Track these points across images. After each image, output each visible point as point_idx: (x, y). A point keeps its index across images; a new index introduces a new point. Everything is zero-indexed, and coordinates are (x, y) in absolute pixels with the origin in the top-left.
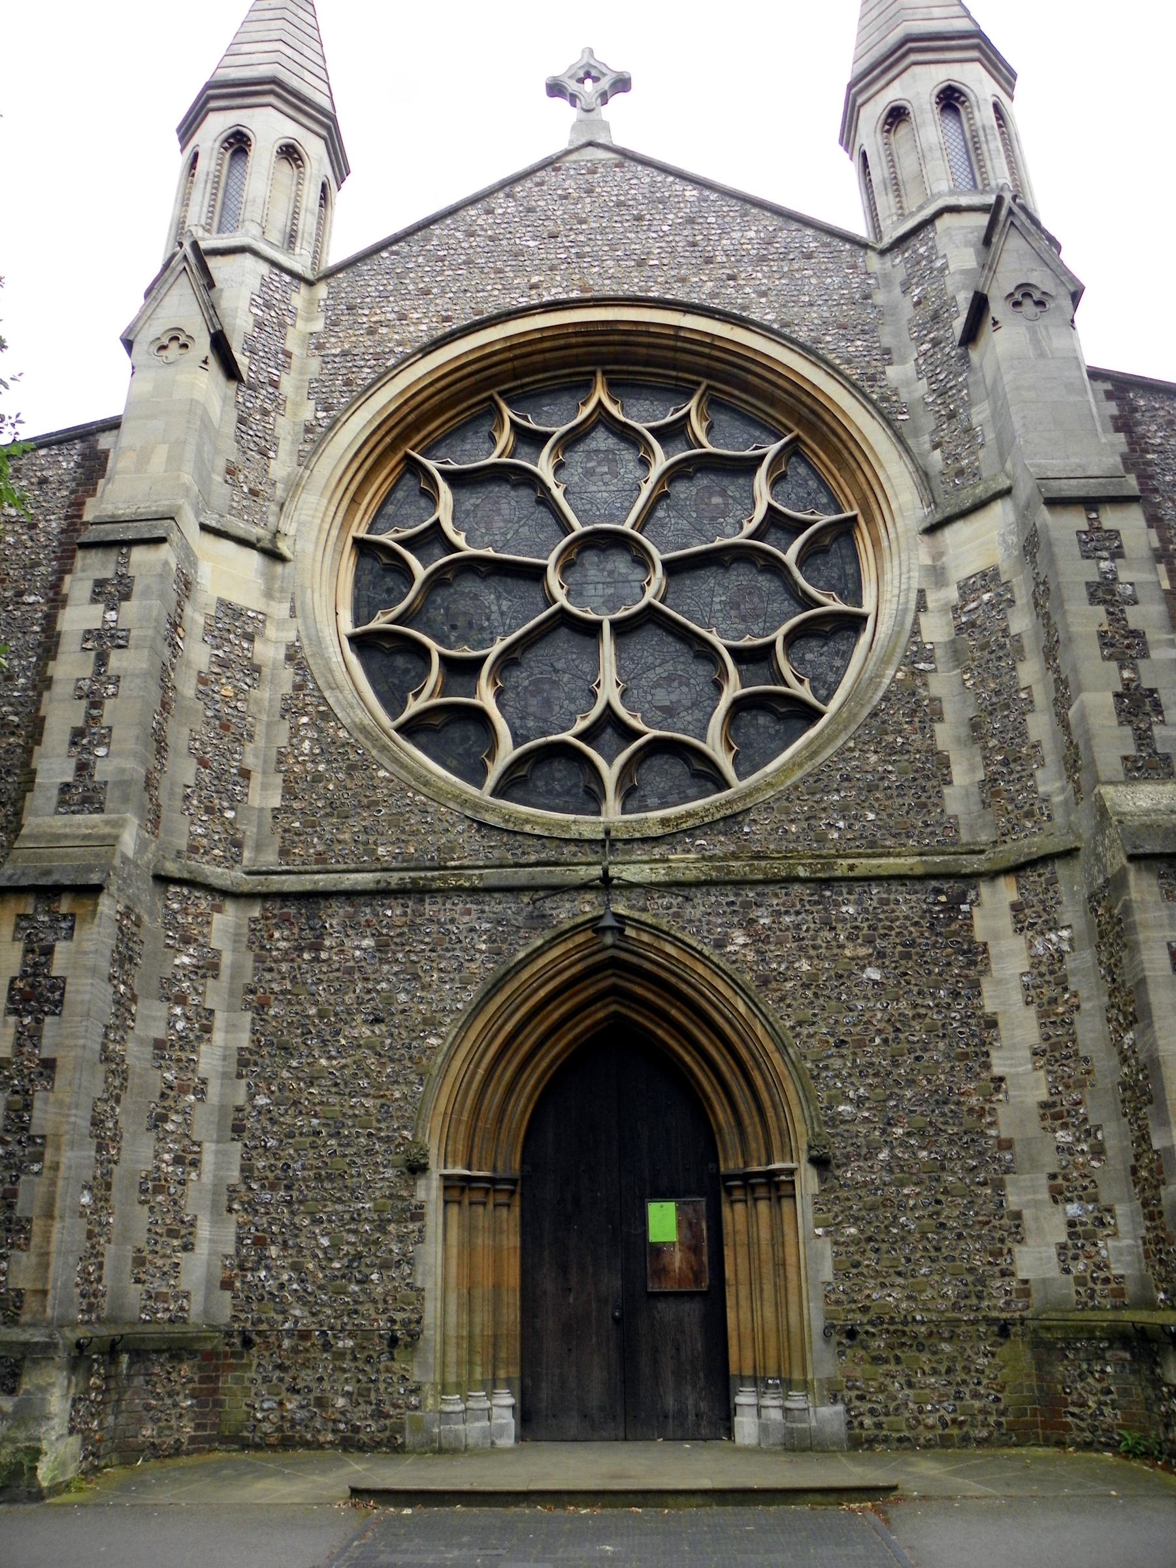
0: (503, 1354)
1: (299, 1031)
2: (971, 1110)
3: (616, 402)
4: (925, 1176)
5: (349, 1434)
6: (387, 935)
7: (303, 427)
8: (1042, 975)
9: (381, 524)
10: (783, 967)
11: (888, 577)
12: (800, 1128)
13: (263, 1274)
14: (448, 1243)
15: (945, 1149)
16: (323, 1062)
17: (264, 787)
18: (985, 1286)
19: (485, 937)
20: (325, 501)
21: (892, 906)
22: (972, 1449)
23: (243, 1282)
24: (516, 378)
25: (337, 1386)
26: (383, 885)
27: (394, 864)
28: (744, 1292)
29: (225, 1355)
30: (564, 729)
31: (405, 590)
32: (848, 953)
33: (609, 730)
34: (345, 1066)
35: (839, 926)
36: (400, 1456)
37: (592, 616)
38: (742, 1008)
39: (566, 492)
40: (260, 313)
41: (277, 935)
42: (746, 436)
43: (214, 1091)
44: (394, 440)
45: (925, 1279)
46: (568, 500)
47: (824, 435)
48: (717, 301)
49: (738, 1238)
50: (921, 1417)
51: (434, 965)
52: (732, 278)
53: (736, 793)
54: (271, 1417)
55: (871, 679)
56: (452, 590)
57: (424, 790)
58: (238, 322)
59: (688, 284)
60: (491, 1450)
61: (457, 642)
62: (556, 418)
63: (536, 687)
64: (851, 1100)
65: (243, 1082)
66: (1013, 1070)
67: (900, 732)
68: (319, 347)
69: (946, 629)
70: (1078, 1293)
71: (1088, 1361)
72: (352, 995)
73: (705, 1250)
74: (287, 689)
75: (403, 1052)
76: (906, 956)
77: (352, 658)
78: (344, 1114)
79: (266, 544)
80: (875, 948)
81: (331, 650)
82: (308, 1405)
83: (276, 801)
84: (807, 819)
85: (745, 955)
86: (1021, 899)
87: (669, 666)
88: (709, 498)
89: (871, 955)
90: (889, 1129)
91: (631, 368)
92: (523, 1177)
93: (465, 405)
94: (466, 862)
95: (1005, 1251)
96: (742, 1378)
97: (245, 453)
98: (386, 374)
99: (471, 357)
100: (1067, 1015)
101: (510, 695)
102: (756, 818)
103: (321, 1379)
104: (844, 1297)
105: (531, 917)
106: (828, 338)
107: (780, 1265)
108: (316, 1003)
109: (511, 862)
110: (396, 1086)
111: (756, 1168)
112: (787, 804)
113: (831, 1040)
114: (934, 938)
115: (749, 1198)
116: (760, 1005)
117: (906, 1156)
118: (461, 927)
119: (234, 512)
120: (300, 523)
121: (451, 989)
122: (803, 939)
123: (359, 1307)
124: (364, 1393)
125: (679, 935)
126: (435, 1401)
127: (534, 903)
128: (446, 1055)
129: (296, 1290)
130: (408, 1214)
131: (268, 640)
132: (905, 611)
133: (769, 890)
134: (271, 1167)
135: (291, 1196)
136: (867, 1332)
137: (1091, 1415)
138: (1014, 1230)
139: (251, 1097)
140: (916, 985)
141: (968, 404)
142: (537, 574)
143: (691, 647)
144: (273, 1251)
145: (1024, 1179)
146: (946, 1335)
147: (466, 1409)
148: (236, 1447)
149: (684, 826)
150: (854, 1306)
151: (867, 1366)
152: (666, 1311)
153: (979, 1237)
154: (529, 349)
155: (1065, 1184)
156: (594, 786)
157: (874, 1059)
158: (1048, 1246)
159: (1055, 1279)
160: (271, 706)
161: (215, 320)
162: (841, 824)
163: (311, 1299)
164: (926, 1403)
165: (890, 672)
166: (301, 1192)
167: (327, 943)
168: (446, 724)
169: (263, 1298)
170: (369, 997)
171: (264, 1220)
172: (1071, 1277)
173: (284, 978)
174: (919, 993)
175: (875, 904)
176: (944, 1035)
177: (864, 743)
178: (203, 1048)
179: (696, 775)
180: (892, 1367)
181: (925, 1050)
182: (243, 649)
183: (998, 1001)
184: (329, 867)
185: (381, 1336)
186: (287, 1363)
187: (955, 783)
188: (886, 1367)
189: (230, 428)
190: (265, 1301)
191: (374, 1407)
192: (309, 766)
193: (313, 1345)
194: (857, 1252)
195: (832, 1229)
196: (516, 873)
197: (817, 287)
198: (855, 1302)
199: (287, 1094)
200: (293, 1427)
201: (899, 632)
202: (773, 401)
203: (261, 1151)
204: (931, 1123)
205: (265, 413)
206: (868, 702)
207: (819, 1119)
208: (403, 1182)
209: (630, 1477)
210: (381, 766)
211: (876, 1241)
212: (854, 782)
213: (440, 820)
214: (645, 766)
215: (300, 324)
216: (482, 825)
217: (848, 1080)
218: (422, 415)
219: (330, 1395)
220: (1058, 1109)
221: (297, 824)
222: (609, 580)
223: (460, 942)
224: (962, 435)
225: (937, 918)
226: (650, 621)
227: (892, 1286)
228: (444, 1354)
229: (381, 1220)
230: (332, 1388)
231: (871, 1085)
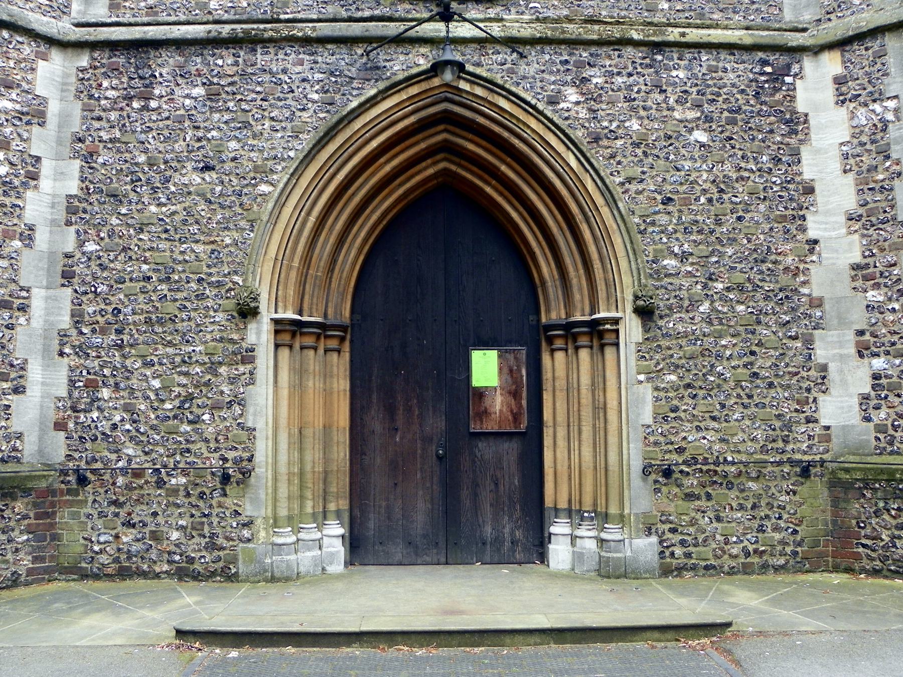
0: (333, 489)
1: (129, 179)
2: (786, 269)
4: (741, 329)
5: (184, 565)
6: (219, 84)
8: (862, 144)
10: (615, 125)
12: (627, 280)
13: (95, 415)
14: (279, 384)
15: (762, 304)
16: (153, 209)
18: (791, 431)
19: (317, 87)
21: (720, 73)
22: (770, 576)
23: (76, 423)
25: (171, 520)
26: (214, 34)
27: (226, 17)
28: (561, 433)
29: (62, 493)
32: (677, 115)
34: (174, 213)
35: (670, 89)
36: (235, 585)
38: (573, 163)
41: (105, 84)
43: (42, 238)
45: (737, 424)
49: (557, 384)
50: (726, 548)
51: (266, 114)
54: (108, 549)
60: (321, 575)
64: (676, 255)
65: (72, 229)
66: (827, 234)
70: (877, 439)
71: (886, 500)
72: (182, 143)
73: (524, 394)
75: (233, 198)
76: (733, 122)
78: (174, 260)
80: (703, 112)
82: (144, 538)
85: (577, 113)
86: (845, 72)
89: (699, 119)
90: (710, 284)
92: (352, 325)
95: (811, 400)
96: (556, 510)
100: (887, 182)
103: (155, 514)
104: (662, 439)
105: (365, 68)
107: (600, 409)
108: (146, 150)
110: (226, 233)
111: (579, 318)
113: (659, 197)
114: (759, 106)
115: (570, 346)
116: (592, 160)
117: (725, 310)
118: (293, 77)
121: (282, 137)
122: (634, 99)
123: (190, 446)
124: (197, 527)
125: (513, 89)
126: (267, 533)
127: (367, 55)
128: (277, 201)
129: (128, 431)
130: (240, 358)
133: (602, 51)
134: (102, 312)
135: (122, 340)
136: (681, 472)
137: (883, 547)
138: (819, 381)
139: (81, 244)
140: (740, 149)
144: (105, 393)
145: (832, 335)
146: (754, 475)
147: (298, 540)
148: (75, 577)
150: (671, 447)
151: (680, 502)
152: (485, 449)
153: (789, 387)
155: (872, 340)
157: (699, 218)
158: (851, 396)
159: (853, 426)
163: (144, 439)
164: (732, 536)
166: (132, 336)
167: (157, 92)
169: (96, 439)
170: (200, 144)
171: (96, 363)
172: (871, 424)
173: (113, 127)
174: (743, 157)
175: (704, 70)
176: (765, 197)
178: (29, 194)
180: (702, 503)
181: (747, 211)
183: (815, 169)
184: (160, 19)
185: (213, 474)
186: (122, 499)
188: (697, 503)
190: (99, 441)
191: (207, 540)
193: (147, 482)
194: (676, 397)
195: (653, 375)
196: (349, 26)
198: (672, 443)
199: (117, 240)
200: (129, 558)
203: (91, 296)
204: (749, 279)
207: (645, 271)
208: (233, 326)
209: (461, 612)
211: (693, 387)
217: (674, 236)
219: (165, 529)
220: (871, 270)
223: (293, 91)
225: (762, 88)
227: (707, 429)
228: (275, 489)
229: (212, 363)
230: (167, 522)
231: (695, 241)
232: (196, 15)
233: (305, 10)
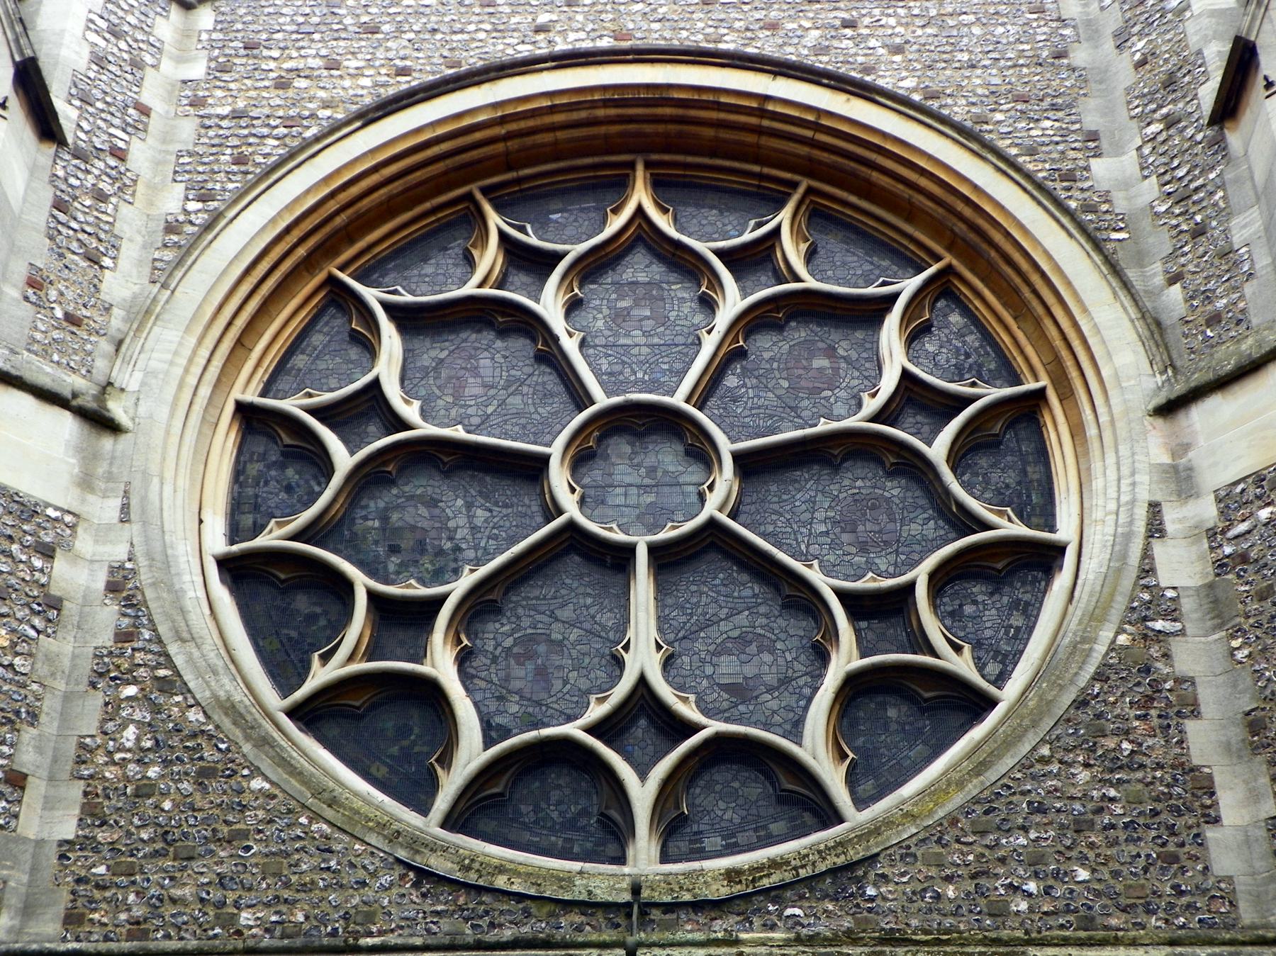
3: (665, 211)
7: (162, 225)
9: (283, 383)
11: (1098, 484)
17: (49, 804)
20: (193, 341)
24: (510, 168)
30: (570, 719)
31: (317, 488)
33: (643, 722)
37: (619, 536)
39: (583, 344)
40: (102, 43)
42: (867, 267)
44: (311, 254)
46: (585, 357)
47: (992, 266)
48: (825, 59)
52: (848, 24)
53: (853, 830)
55: (1074, 646)
56: (395, 491)
57: (329, 813)
58: (64, 52)
59: (782, 33)
61: (398, 573)
62: (570, 231)
63: (526, 648)
67: (1126, 733)
68: (197, 103)
69: (1198, 567)
74: (105, 639)
77: (222, 594)
79: (88, 402)
81: (187, 578)
83: (68, 830)
84: (974, 877)
87: (743, 619)
88: (809, 359)
91: (690, 159)
93: (427, 205)
94: (392, 939)
97: (61, 256)
98: (302, 149)
99: (440, 131)
101: (480, 661)
102: (886, 871)
106: (999, 116)
109: (470, 940)
112: (938, 849)
119: (36, 347)
120: (148, 373)
131: (78, 557)
132: (1128, 536)
141: (1225, 213)
142: (535, 467)
143: (778, 589)
149: (766, 883)
154: (531, 123)
156: (614, 814)
160: (74, 667)
161: (23, 41)
162: (1032, 886)
165: (1106, 634)
168: (373, 707)
177: (1067, 750)
179: (785, 799)
182: (33, 569)
187: (1225, 821)
189: (40, 215)
192: (132, 768)
197: (983, 40)
201: (1119, 571)
202: (910, 213)
205: (101, 197)
206: (1072, 682)
210: (256, 772)
212: (1052, 815)
213: (352, 865)
214: (702, 783)
215: (166, 65)
216: (424, 874)
218: (359, 216)
221: (101, 870)
222: (647, 481)
224: (1216, 262)
226: (713, 546)
232: (216, 936)
233: (402, 928)
